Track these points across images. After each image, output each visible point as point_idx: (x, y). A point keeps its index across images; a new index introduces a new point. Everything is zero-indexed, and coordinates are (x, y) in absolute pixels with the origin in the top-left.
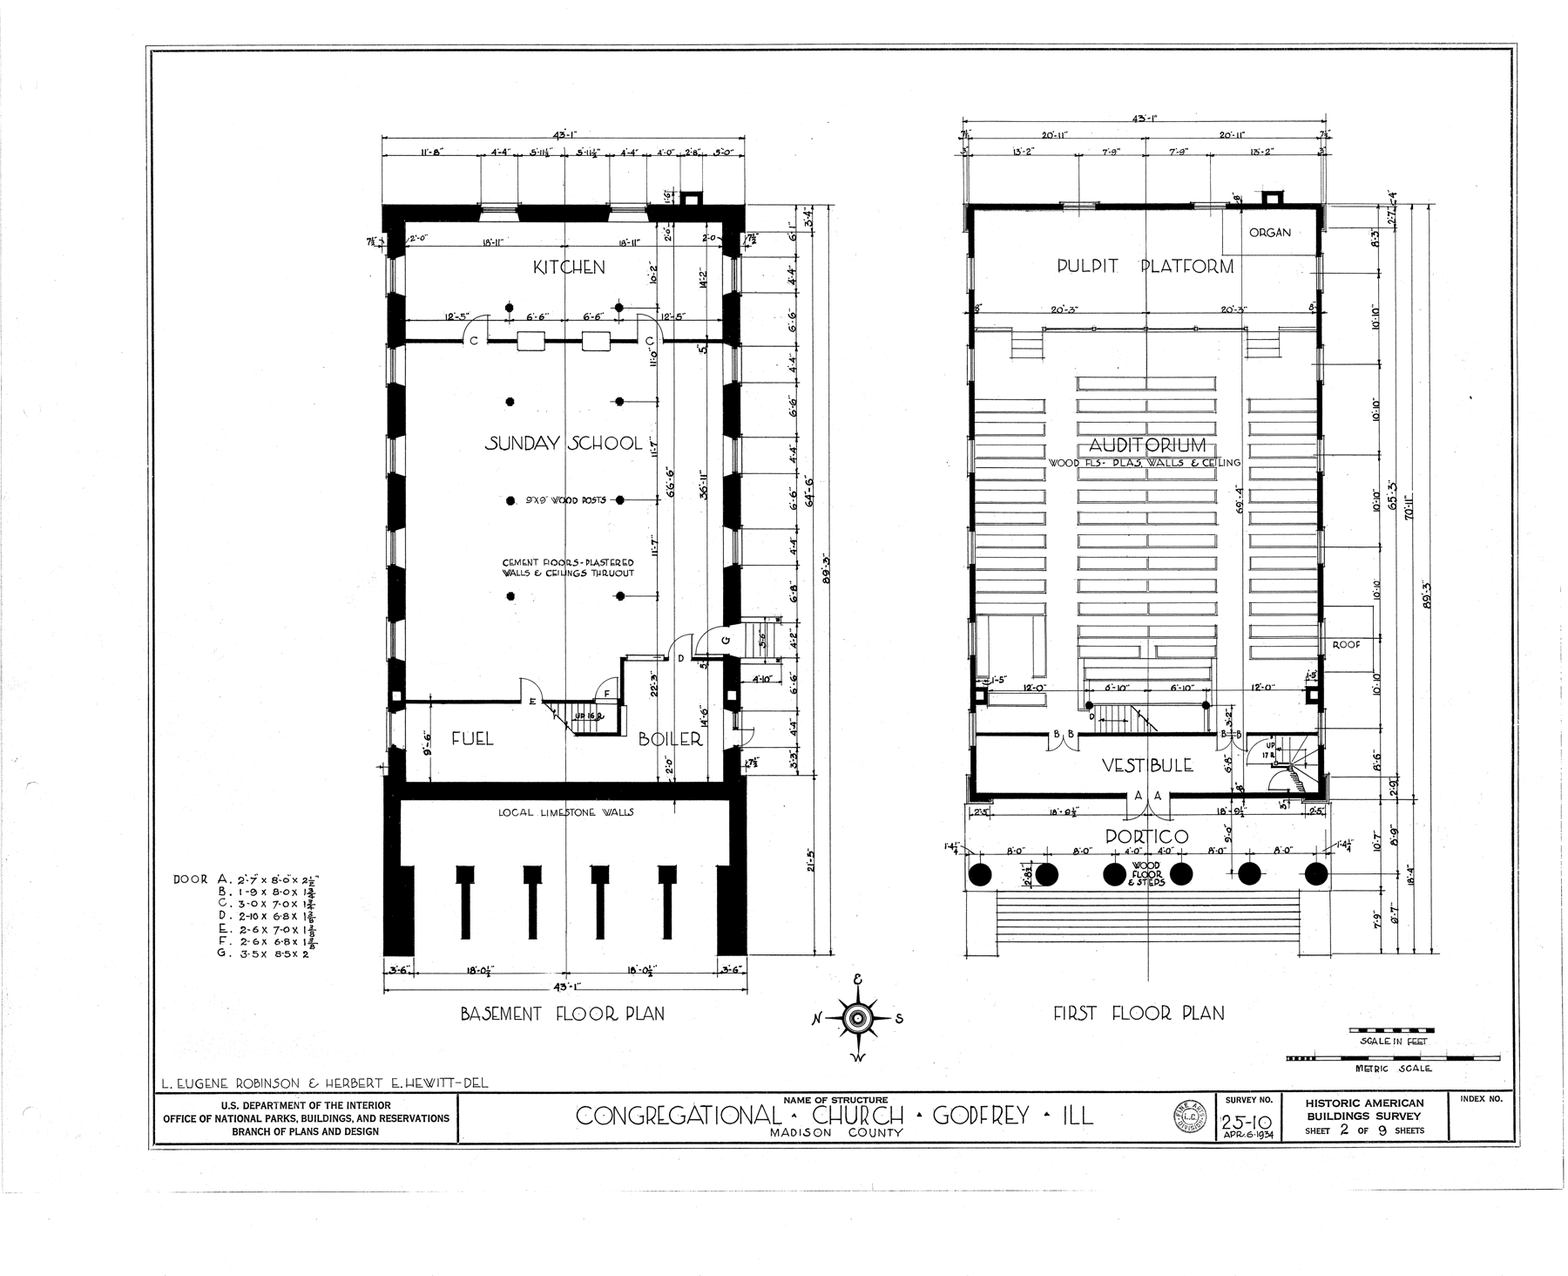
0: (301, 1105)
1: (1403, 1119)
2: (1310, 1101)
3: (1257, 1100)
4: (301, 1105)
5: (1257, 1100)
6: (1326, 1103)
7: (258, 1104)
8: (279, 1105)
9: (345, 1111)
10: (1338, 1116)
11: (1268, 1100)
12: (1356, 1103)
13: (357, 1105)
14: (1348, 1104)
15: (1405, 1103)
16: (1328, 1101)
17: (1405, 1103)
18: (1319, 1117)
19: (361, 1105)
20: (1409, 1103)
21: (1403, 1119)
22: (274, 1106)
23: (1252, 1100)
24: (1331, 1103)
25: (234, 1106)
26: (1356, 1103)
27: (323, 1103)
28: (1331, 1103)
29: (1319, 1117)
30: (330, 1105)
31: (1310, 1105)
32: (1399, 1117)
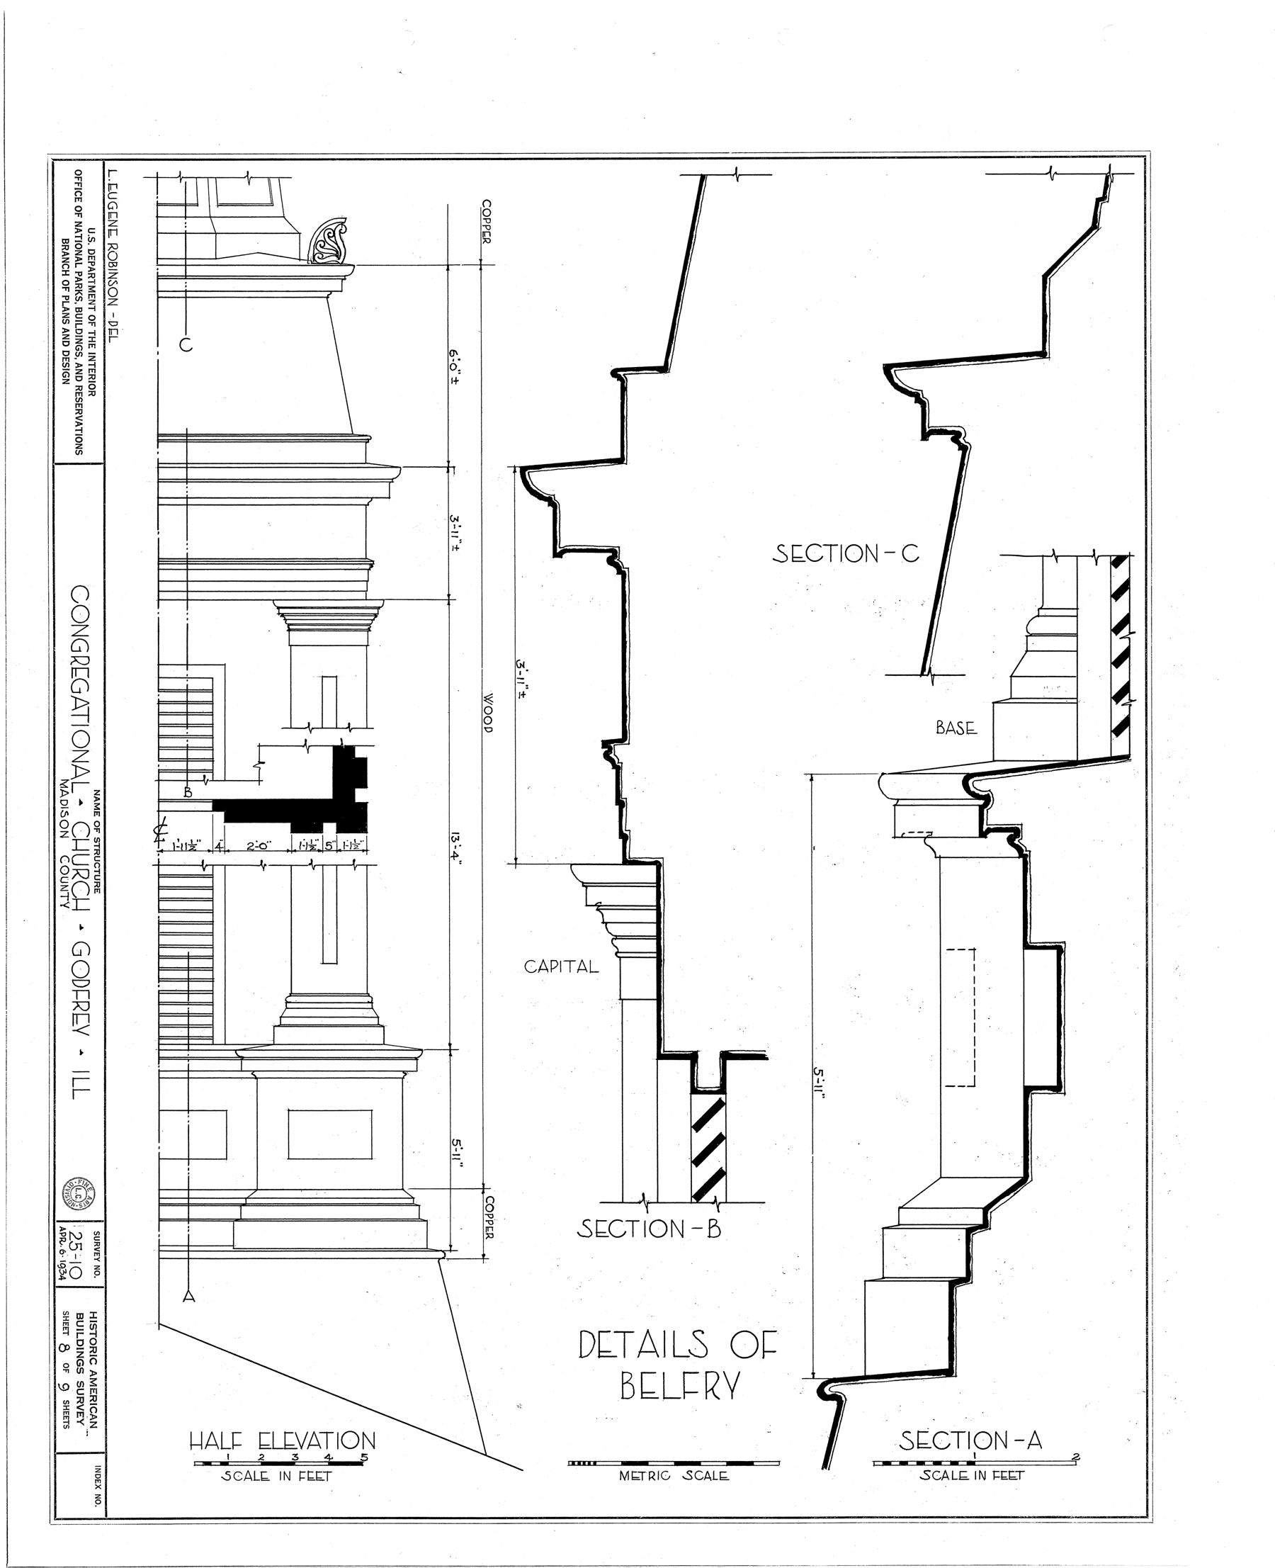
0: (92, 306)
1: (78, 1408)
2: (95, 1315)
3: (97, 1263)
4: (92, 306)
5: (97, 1263)
6: (94, 1331)
7: (93, 263)
8: (92, 284)
9: (86, 351)
10: (80, 1343)
11: (97, 1273)
12: (93, 1361)
13: (93, 363)
14: (92, 1354)
15: (93, 1410)
16: (96, 1334)
17: (93, 1410)
18: (79, 1324)
19: (93, 367)
20: (94, 1414)
21: (78, 1408)
22: (91, 279)
23: (97, 1257)
24: (94, 1336)
25: (91, 240)
26: (93, 1361)
27: (95, 328)
28: (94, 1336)
29: (79, 1324)
30: (93, 335)
31: (92, 1315)
32: (80, 1404)
